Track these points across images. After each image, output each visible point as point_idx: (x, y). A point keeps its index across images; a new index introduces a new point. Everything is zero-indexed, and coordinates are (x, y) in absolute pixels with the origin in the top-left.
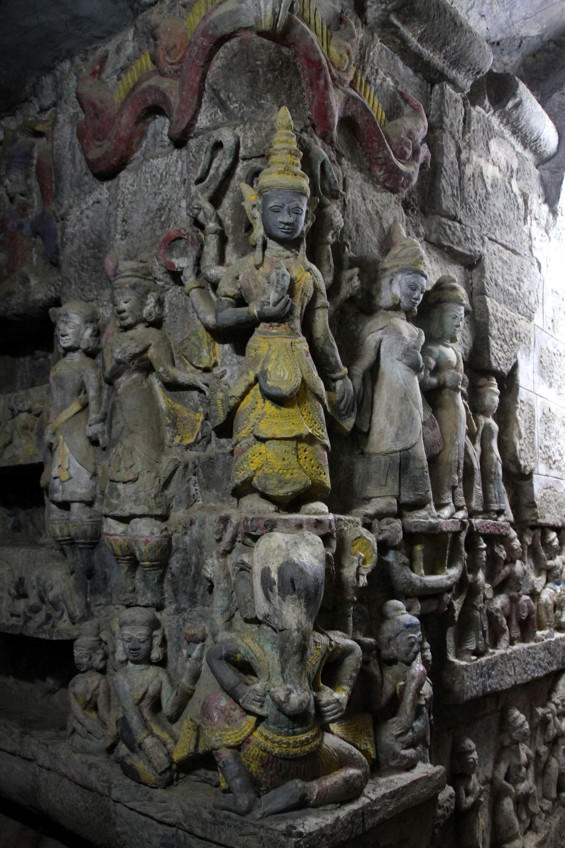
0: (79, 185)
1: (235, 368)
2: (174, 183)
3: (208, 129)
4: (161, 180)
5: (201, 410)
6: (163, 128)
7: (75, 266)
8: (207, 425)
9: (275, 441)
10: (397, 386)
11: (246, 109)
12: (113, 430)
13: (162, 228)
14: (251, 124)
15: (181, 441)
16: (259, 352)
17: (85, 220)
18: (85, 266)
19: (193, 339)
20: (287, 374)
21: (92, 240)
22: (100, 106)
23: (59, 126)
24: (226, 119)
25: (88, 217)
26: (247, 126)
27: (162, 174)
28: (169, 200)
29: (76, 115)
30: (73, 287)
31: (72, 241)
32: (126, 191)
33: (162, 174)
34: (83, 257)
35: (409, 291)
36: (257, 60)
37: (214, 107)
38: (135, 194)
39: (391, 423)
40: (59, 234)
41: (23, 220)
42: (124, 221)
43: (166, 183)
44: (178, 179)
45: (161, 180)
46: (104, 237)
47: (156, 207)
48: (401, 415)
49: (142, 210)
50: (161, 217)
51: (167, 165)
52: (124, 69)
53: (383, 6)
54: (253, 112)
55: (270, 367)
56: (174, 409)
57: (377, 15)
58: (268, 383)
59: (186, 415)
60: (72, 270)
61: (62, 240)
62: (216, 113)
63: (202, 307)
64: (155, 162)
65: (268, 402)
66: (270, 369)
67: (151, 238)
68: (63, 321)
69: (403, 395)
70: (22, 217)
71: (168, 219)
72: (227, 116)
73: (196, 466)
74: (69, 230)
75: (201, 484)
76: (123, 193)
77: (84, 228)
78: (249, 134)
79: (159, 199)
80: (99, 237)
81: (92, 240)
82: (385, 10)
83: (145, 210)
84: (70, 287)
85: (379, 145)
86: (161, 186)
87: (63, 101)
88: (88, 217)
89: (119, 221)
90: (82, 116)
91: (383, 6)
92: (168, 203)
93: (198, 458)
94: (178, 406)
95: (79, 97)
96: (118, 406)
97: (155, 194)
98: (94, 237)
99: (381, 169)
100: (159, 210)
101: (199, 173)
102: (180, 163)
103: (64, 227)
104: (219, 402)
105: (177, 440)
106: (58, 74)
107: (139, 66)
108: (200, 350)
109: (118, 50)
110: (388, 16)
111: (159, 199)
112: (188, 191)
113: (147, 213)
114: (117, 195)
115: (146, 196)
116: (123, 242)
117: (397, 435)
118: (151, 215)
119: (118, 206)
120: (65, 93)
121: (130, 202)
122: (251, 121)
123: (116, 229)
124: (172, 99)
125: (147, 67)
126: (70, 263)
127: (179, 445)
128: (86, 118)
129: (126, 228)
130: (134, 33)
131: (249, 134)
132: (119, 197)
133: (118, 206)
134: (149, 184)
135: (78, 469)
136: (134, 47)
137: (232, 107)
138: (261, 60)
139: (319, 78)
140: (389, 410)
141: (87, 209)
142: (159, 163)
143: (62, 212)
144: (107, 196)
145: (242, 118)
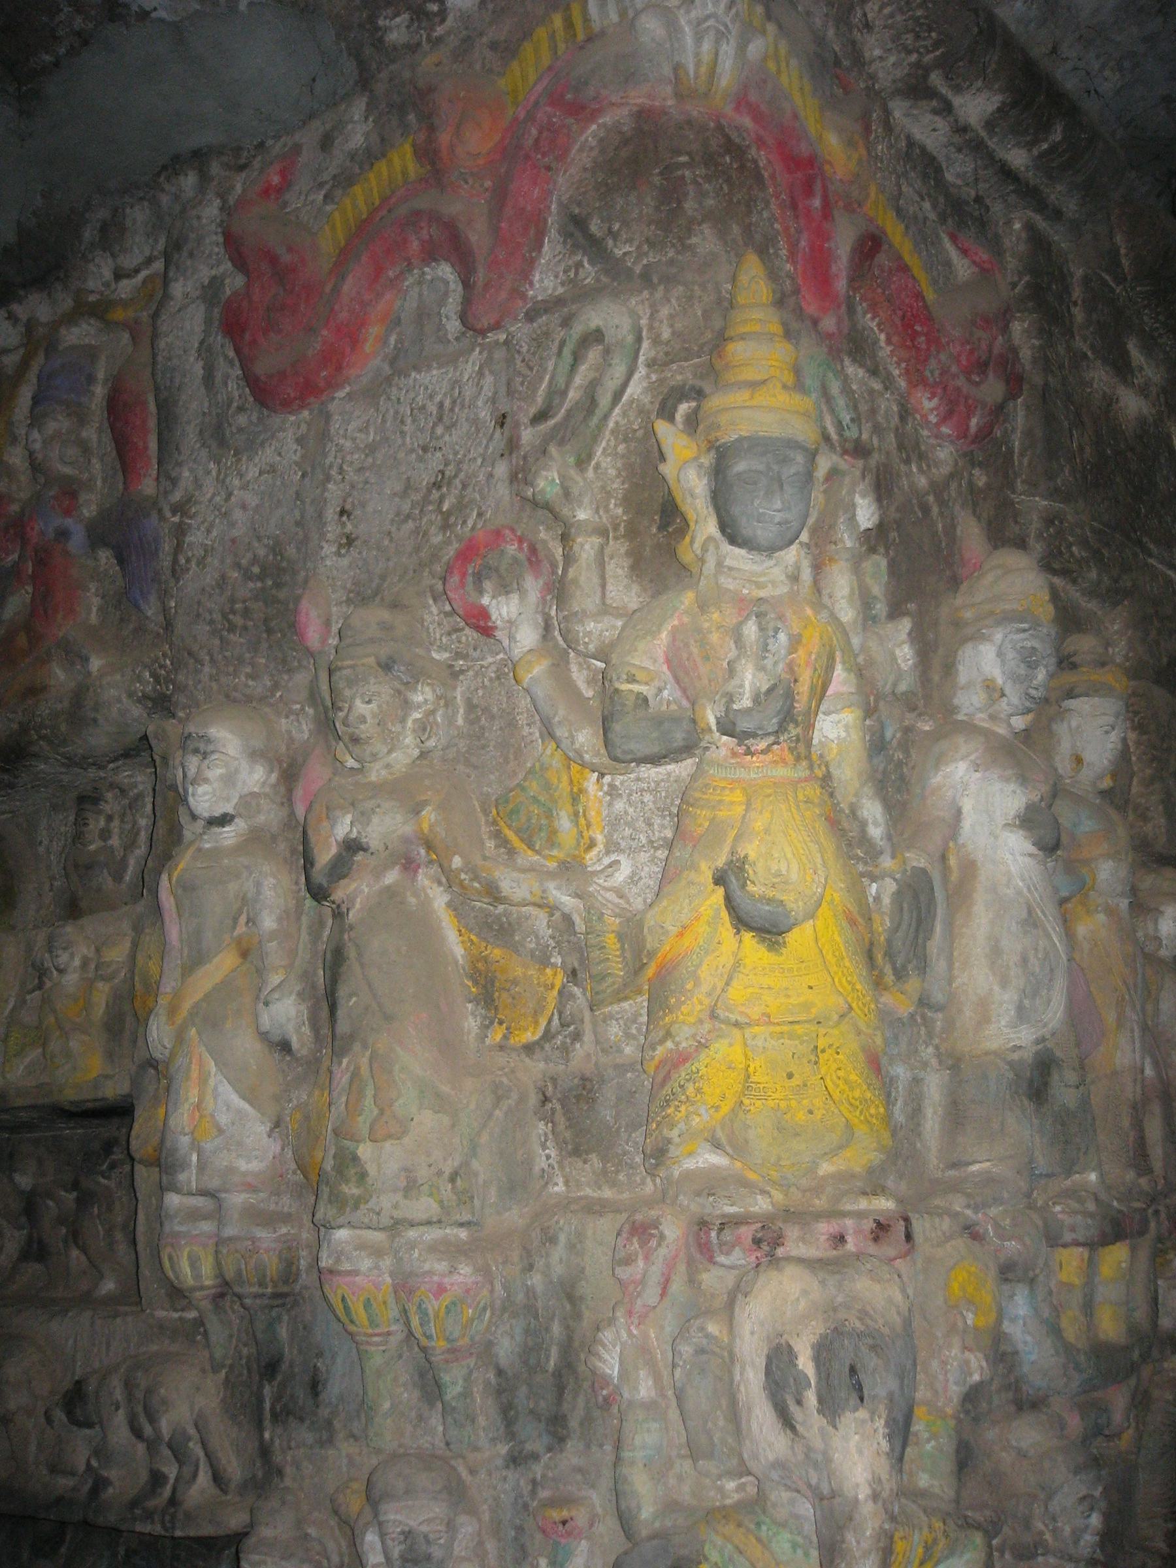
0: (217, 435)
1: (644, 857)
2: (475, 421)
3: (559, 302)
4: (440, 419)
5: (557, 960)
6: (442, 302)
7: (211, 622)
8: (572, 996)
9: (342, 992)
10: (1010, 892)
11: (652, 258)
12: (340, 1013)
13: (445, 526)
14: (667, 290)
15: (505, 1037)
16: (722, 814)
17: (238, 515)
18: (238, 620)
19: (534, 787)
20: (795, 866)
21: (255, 560)
22: (286, 258)
23: (173, 306)
24: (604, 279)
25: (244, 507)
26: (659, 293)
27: (441, 405)
28: (460, 462)
29: (215, 284)
30: (207, 669)
31: (201, 562)
32: (348, 444)
33: (441, 405)
34: (232, 600)
35: (1022, 670)
36: (679, 153)
37: (572, 253)
38: (371, 449)
39: (1004, 983)
40: (167, 547)
41: (69, 522)
42: (343, 512)
43: (454, 425)
44: (485, 414)
45: (440, 419)
46: (291, 551)
47: (426, 479)
48: (1024, 960)
49: (394, 485)
50: (441, 501)
51: (455, 383)
52: (345, 181)
53: (914, 58)
54: (672, 262)
55: (750, 849)
56: (485, 960)
57: (899, 73)
58: (750, 888)
59: (519, 972)
60: (202, 629)
61: (175, 561)
62: (579, 265)
63: (562, 712)
64: (423, 377)
65: (748, 936)
66: (752, 856)
67: (417, 549)
68: (196, 751)
69: (1024, 915)
70: (67, 512)
71: (461, 507)
72: (607, 272)
73: (546, 1100)
74: (196, 538)
75: (561, 1144)
76: (340, 449)
77: (235, 533)
78: (665, 312)
79: (435, 461)
80: (277, 549)
81: (255, 560)
82: (918, 65)
83: (399, 487)
84: (197, 672)
85: (928, 341)
86: (439, 430)
87: (185, 254)
88: (244, 507)
89: (331, 513)
90: (235, 282)
91: (914, 58)
92: (459, 470)
93: (554, 1080)
94: (497, 953)
95: (231, 242)
96: (352, 953)
97: (425, 449)
98: (262, 552)
99: (933, 395)
100: (437, 485)
101: (540, 400)
102: (489, 380)
103: (180, 531)
104: (611, 940)
105: (496, 1035)
106: (165, 199)
107: (385, 174)
108: (549, 815)
109: (326, 143)
110: (926, 77)
111: (435, 461)
112: (512, 445)
113: (404, 494)
114: (325, 455)
115: (401, 455)
116: (345, 562)
117: (1020, 1008)
118: (416, 497)
119: (328, 478)
120: (192, 236)
121: (361, 470)
122: (668, 281)
123: (322, 536)
124: (473, 238)
125: (404, 173)
126: (198, 615)
127: (502, 1048)
128: (248, 285)
129: (349, 527)
130: (368, 104)
131: (665, 312)
132: (330, 459)
133: (328, 478)
134: (408, 427)
135: (239, 1111)
136: (367, 135)
137: (618, 252)
138: (689, 154)
139: (809, 192)
140: (995, 951)
141: (244, 487)
142: (432, 381)
143: (177, 496)
144: (296, 458)
145: (646, 276)
